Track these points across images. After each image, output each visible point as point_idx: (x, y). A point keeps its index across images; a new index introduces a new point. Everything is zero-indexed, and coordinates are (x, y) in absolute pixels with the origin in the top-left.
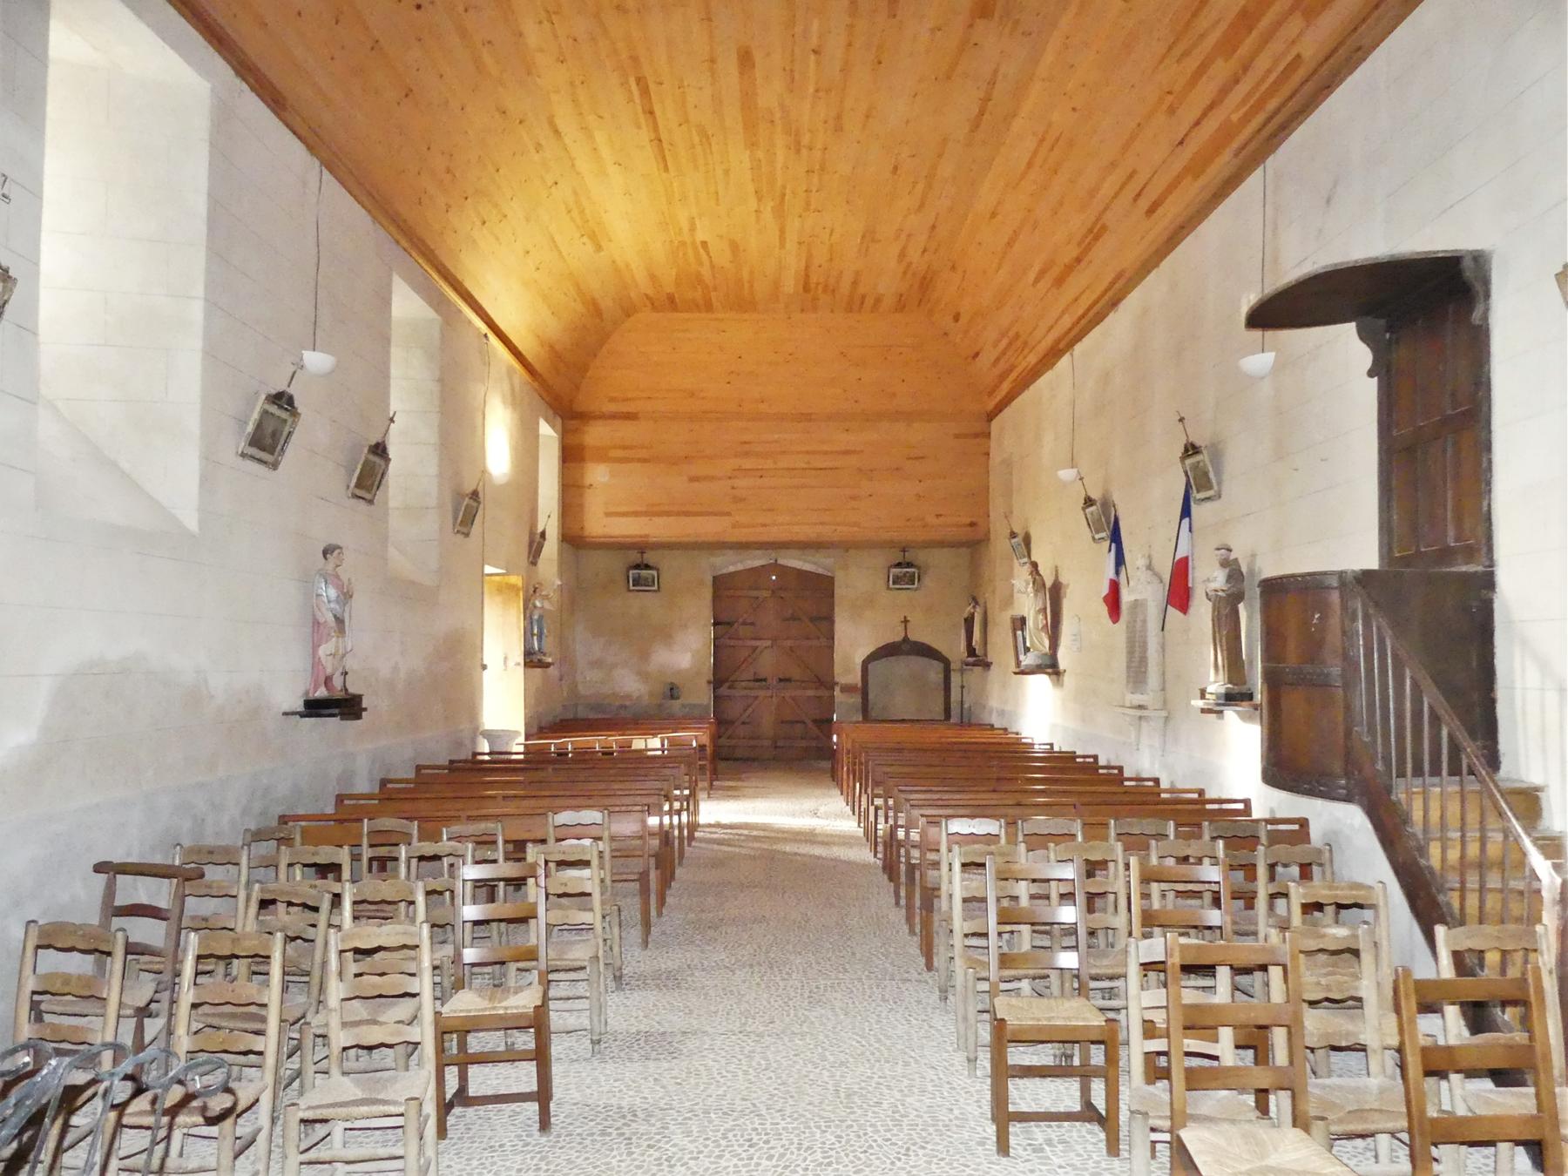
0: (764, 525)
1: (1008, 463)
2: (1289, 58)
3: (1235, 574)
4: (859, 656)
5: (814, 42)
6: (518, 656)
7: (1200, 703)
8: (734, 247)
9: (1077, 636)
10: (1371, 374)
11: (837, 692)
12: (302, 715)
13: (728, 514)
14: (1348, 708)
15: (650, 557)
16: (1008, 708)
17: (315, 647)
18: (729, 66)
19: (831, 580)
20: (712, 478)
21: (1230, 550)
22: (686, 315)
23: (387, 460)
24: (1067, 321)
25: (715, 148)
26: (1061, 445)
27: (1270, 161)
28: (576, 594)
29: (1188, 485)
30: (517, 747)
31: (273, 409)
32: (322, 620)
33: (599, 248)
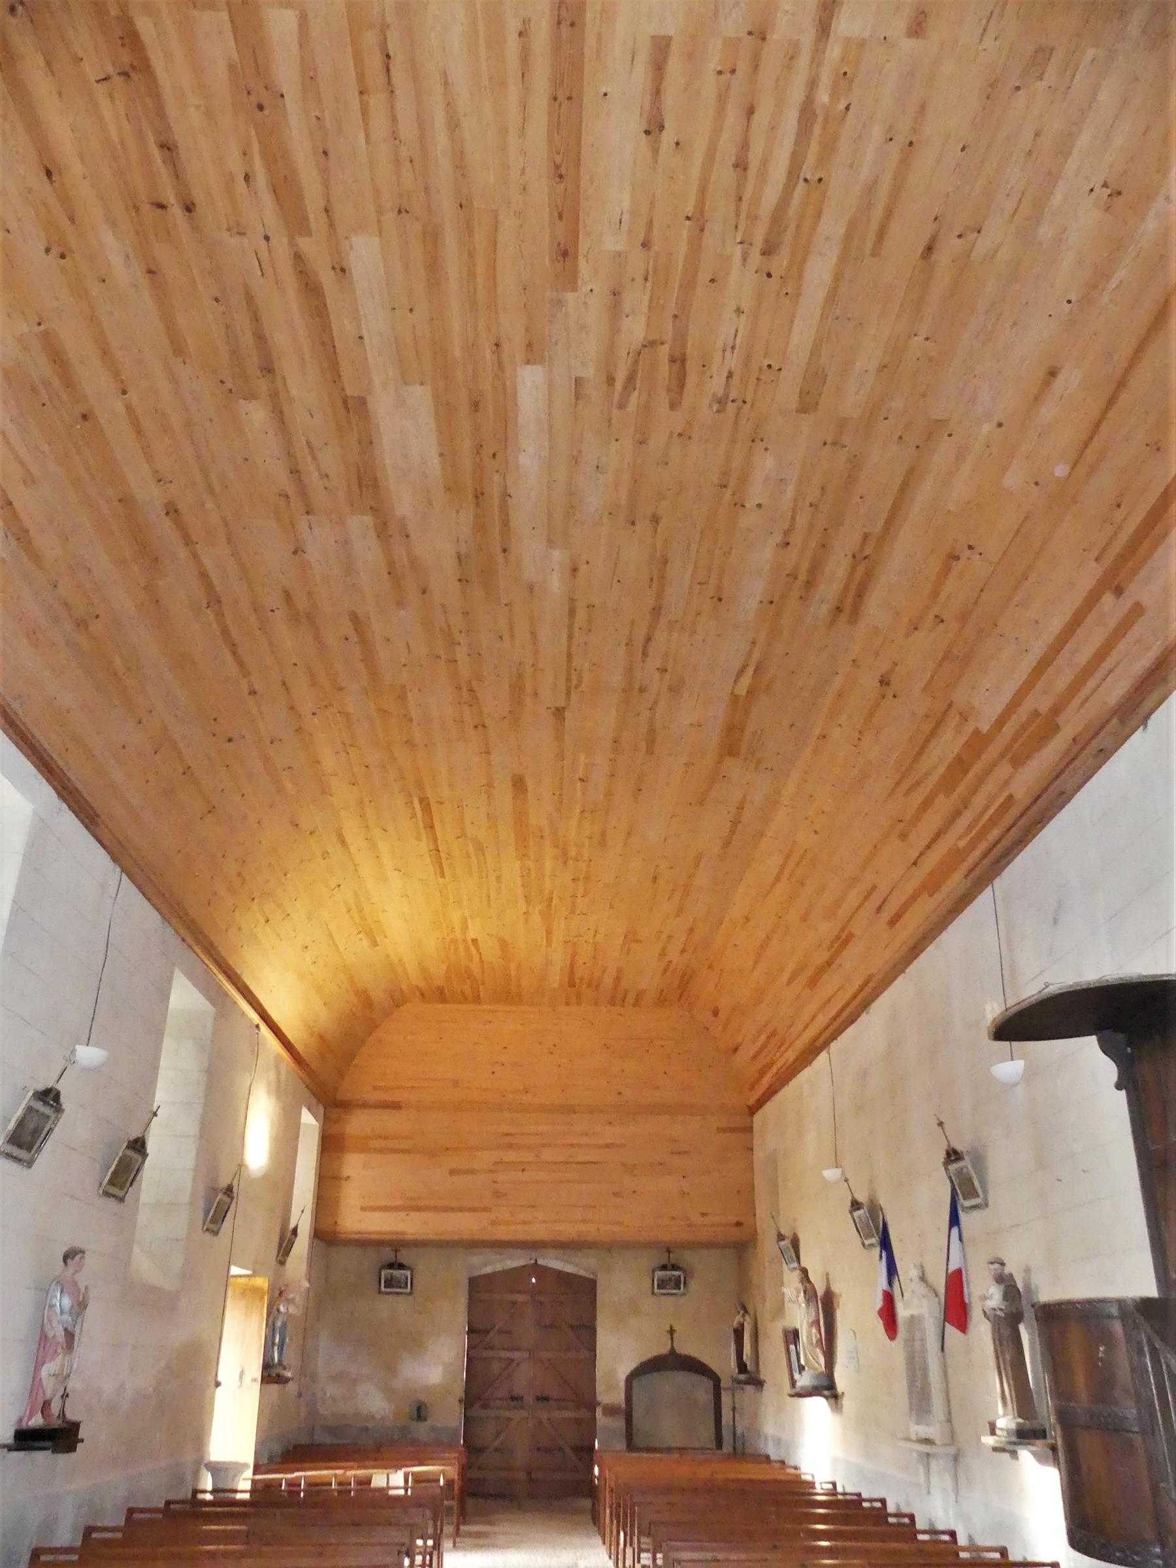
0: (525, 1223)
1: (772, 1160)
2: (1001, 799)
3: (1011, 1291)
4: (623, 1371)
5: (581, 773)
6: (256, 1370)
7: (989, 1440)
8: (503, 944)
9: (855, 1355)
10: (1119, 1086)
11: (599, 1412)
12: (10, 1448)
13: (486, 1209)
14: (1151, 1460)
15: (404, 1256)
16: (784, 1437)
17: (38, 1366)
18: (504, 790)
19: (593, 1283)
20: (472, 1172)
21: (1003, 1264)
22: (456, 1006)
23: (144, 1155)
24: (822, 1020)
25: (489, 859)
26: (823, 1146)
27: (997, 882)
28: (326, 1292)
29: (954, 1190)
30: (244, 1485)
31: (39, 1106)
32: (50, 1334)
33: (375, 943)
